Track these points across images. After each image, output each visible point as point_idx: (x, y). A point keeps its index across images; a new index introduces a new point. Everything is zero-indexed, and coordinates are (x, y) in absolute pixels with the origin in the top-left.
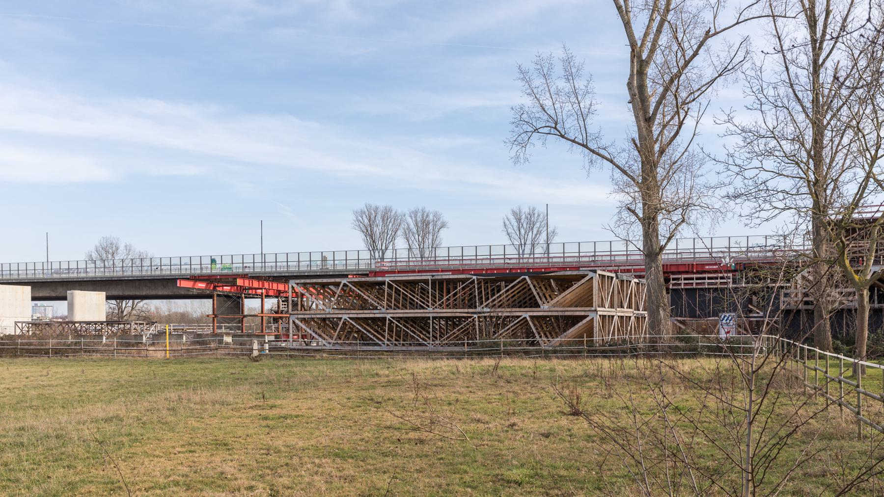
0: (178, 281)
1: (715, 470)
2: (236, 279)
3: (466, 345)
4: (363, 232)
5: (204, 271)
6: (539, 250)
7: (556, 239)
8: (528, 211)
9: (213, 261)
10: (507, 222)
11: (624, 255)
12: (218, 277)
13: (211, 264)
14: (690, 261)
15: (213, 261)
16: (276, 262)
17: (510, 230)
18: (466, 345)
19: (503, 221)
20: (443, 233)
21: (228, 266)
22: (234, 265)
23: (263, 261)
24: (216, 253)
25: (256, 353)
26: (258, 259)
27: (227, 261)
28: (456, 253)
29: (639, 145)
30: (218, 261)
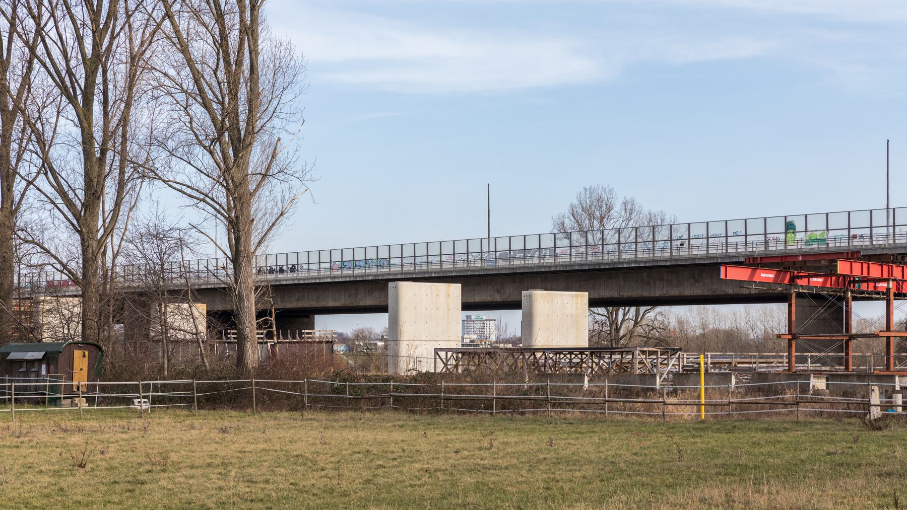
9: (789, 227)
12: (800, 259)
13: (786, 233)
15: (789, 227)
21: (818, 235)
23: (891, 223)
24: (794, 209)
26: (880, 219)
27: (817, 224)
30: (800, 225)
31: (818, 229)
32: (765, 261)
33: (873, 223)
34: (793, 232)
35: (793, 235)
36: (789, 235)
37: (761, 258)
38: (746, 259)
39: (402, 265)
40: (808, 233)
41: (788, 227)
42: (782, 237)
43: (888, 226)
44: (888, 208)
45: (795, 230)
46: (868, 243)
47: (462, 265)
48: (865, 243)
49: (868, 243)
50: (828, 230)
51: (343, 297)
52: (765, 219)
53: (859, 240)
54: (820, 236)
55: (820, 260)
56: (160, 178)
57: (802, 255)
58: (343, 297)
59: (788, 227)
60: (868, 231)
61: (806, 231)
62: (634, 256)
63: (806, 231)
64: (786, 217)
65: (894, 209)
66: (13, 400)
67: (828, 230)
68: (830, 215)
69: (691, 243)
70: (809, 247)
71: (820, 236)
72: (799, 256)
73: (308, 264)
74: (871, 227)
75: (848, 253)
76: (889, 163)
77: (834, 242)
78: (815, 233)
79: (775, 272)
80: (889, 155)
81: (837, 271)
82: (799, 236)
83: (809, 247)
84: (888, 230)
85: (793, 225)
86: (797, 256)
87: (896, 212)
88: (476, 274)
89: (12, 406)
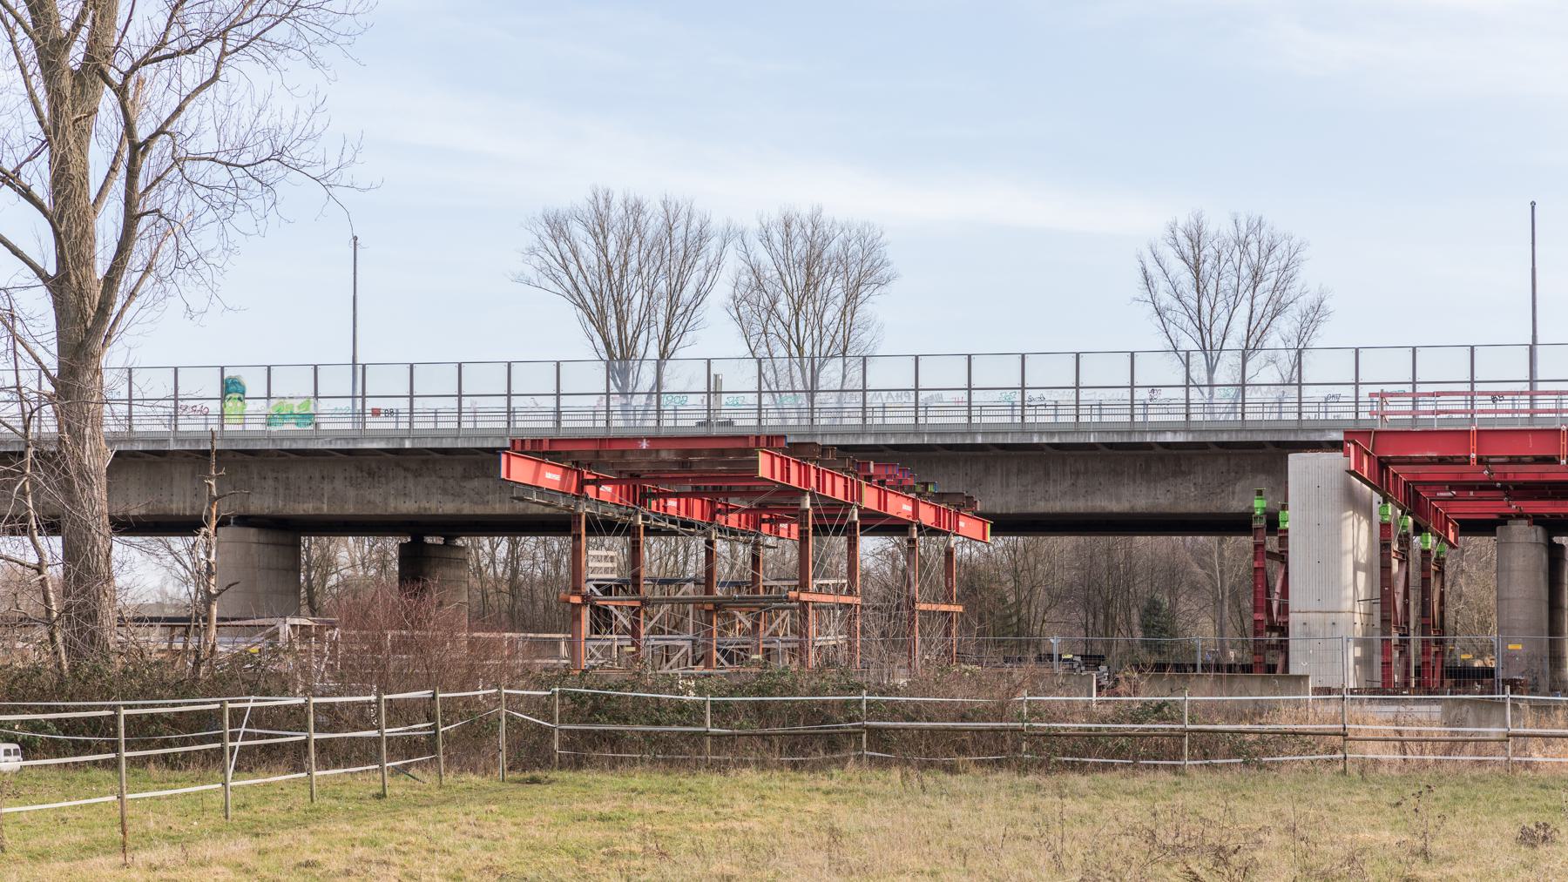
0: (504, 458)
1: (1217, 855)
2: (751, 452)
3: (40, 577)
4: (584, 306)
5: (187, 426)
6: (1263, 371)
7: (1324, 335)
8: (1233, 233)
9: (231, 388)
10: (1153, 270)
11: (1522, 393)
12: (644, 445)
13: (223, 399)
14: (1459, 422)
15: (231, 388)
16: (1132, 387)
17: (1166, 299)
18: (40, 577)
19: (1139, 266)
20: (874, 307)
21: (296, 406)
22: (323, 405)
23: (359, 392)
24: (242, 357)
25: (633, 649)
26: (337, 382)
27: (292, 386)
28: (1386, 369)
29: (46, 114)
30: (254, 385)
31: (295, 395)
32: (558, 447)
33: (415, 390)
34: (239, 399)
35: (239, 404)
36: (229, 404)
37: (551, 441)
38: (513, 441)
39: (558, 412)
40: (274, 402)
41: (227, 387)
42: (214, 407)
43: (354, 397)
44: (354, 363)
45: (243, 393)
46: (406, 426)
47: (1008, 420)
48: (401, 426)
49: (406, 426)
50: (316, 397)
51: (999, 470)
52: (176, 369)
53: (385, 419)
54: (299, 407)
55: (658, 451)
56: (269, 159)
57: (648, 439)
58: (999, 470)
59: (227, 387)
60: (403, 404)
61: (269, 397)
62: (754, 423)
63: (269, 397)
64: (222, 368)
65: (364, 366)
66: (124, 761)
67: (316, 397)
68: (514, 367)
69: (513, 405)
70: (274, 429)
71: (299, 407)
72: (641, 439)
73: (1357, 384)
74: (411, 396)
75: (758, 438)
76: (1536, 266)
77: (433, 419)
78: (289, 401)
79: (561, 470)
80: (358, 261)
81: (757, 472)
82: (251, 406)
83: (274, 429)
84: (354, 405)
85: (239, 383)
86: (640, 439)
87: (179, 374)
88: (892, 442)
89: (224, 771)
